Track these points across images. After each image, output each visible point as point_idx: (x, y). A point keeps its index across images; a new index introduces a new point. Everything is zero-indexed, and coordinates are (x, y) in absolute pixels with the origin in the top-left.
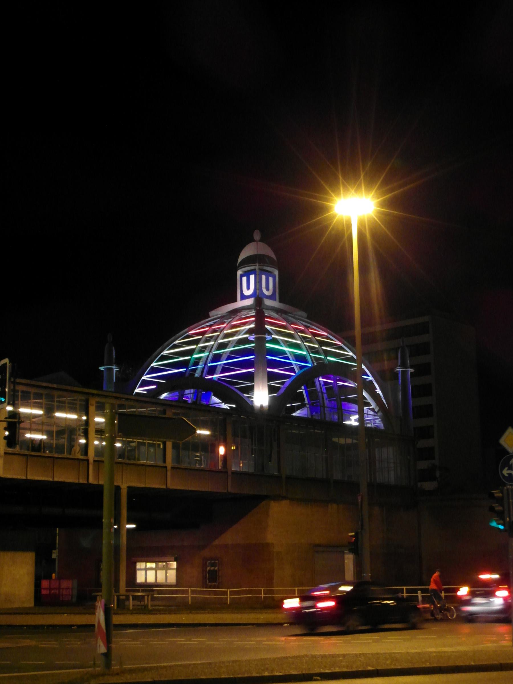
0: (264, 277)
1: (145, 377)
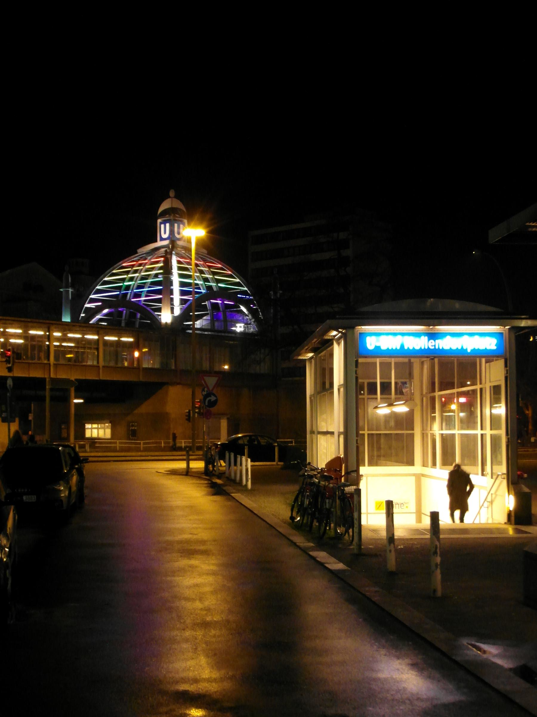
0: (176, 225)
1: (92, 296)
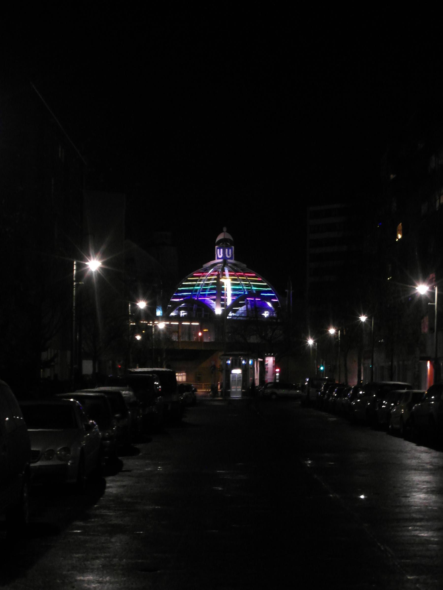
0: (227, 250)
